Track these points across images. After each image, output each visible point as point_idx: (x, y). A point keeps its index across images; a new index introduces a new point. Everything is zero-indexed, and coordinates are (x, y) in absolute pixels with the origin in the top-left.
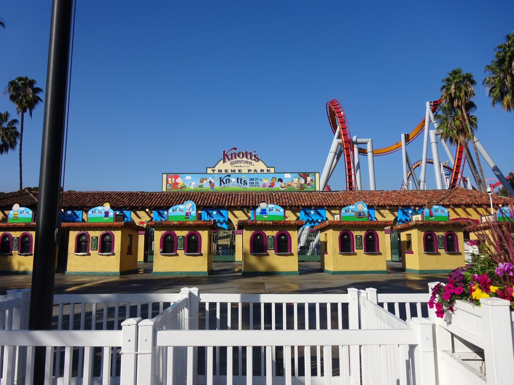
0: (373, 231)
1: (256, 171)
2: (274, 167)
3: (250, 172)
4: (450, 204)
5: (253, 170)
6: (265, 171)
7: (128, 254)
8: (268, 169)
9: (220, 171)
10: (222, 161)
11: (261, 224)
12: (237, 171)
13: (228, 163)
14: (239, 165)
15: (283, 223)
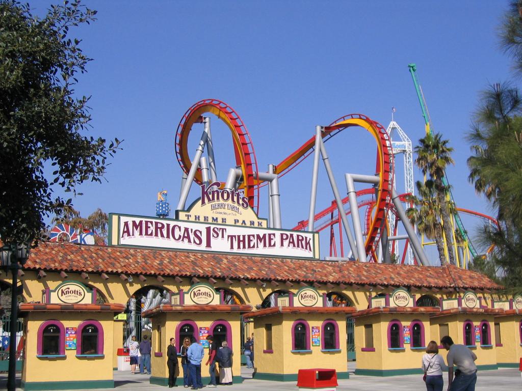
0: (304, 320)
1: (244, 222)
2: (266, 219)
3: (237, 224)
4: (40, 268)
5: (241, 222)
6: (256, 225)
7: (265, 352)
8: (260, 221)
9: (197, 218)
10: (200, 201)
11: (477, 312)
12: (220, 221)
13: (208, 205)
14: (222, 210)
15: (491, 312)
